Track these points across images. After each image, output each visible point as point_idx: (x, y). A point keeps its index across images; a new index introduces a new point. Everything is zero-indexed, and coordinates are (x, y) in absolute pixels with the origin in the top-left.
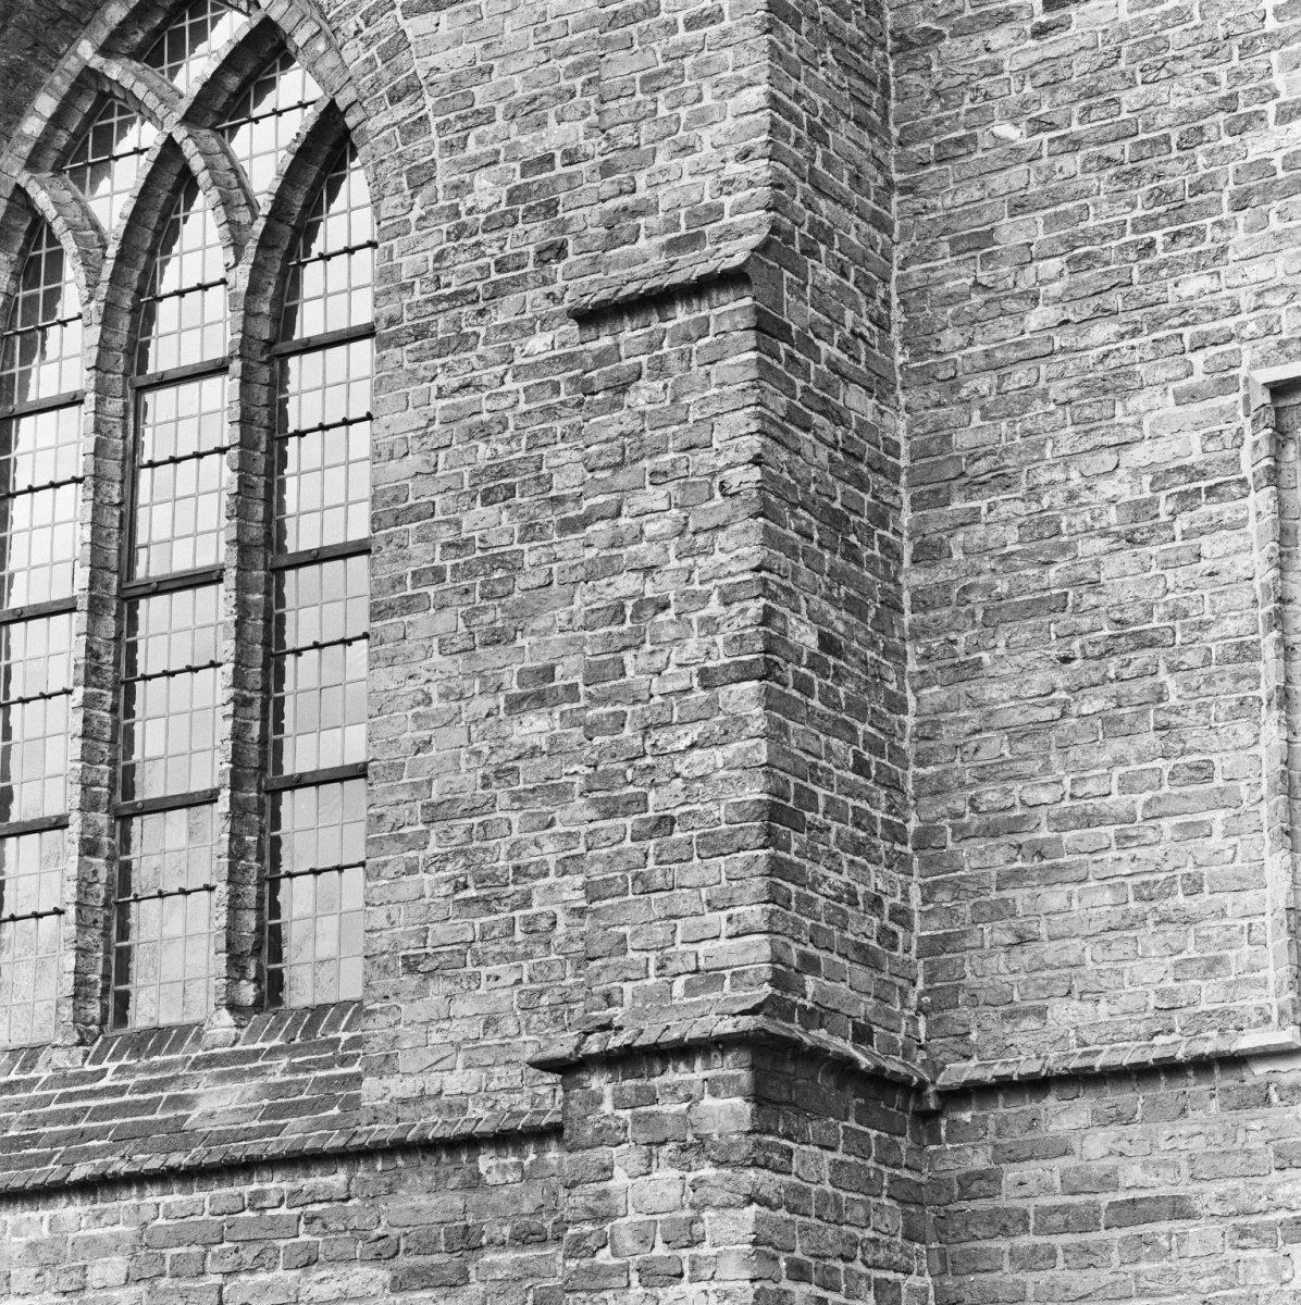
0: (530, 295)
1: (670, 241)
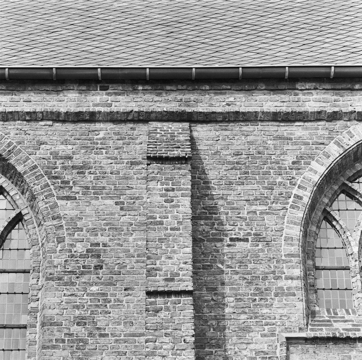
0: (92, 276)
1: (166, 279)
